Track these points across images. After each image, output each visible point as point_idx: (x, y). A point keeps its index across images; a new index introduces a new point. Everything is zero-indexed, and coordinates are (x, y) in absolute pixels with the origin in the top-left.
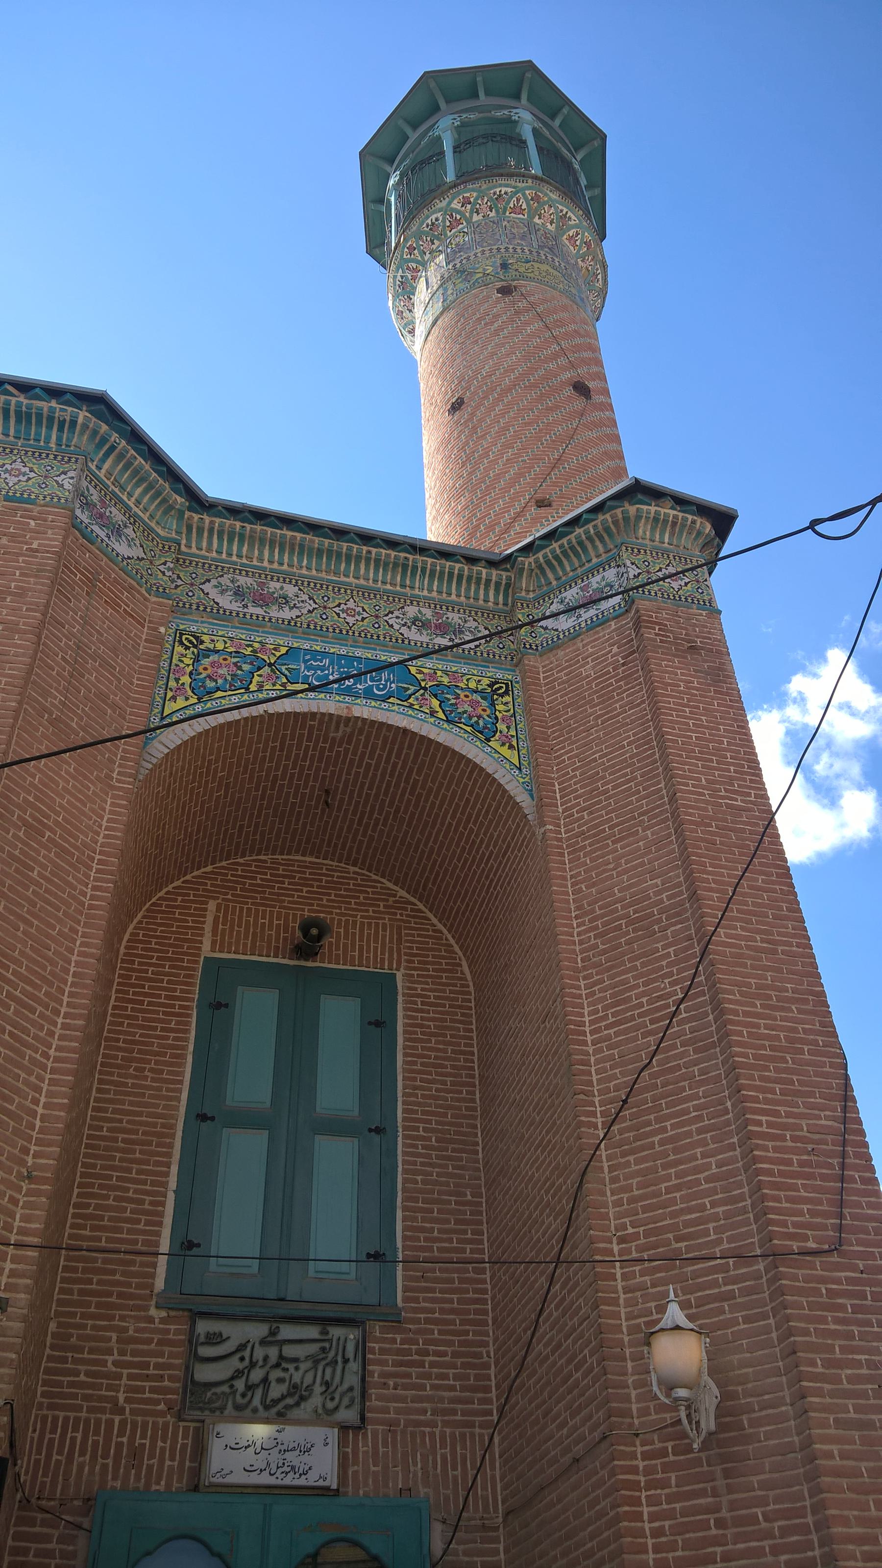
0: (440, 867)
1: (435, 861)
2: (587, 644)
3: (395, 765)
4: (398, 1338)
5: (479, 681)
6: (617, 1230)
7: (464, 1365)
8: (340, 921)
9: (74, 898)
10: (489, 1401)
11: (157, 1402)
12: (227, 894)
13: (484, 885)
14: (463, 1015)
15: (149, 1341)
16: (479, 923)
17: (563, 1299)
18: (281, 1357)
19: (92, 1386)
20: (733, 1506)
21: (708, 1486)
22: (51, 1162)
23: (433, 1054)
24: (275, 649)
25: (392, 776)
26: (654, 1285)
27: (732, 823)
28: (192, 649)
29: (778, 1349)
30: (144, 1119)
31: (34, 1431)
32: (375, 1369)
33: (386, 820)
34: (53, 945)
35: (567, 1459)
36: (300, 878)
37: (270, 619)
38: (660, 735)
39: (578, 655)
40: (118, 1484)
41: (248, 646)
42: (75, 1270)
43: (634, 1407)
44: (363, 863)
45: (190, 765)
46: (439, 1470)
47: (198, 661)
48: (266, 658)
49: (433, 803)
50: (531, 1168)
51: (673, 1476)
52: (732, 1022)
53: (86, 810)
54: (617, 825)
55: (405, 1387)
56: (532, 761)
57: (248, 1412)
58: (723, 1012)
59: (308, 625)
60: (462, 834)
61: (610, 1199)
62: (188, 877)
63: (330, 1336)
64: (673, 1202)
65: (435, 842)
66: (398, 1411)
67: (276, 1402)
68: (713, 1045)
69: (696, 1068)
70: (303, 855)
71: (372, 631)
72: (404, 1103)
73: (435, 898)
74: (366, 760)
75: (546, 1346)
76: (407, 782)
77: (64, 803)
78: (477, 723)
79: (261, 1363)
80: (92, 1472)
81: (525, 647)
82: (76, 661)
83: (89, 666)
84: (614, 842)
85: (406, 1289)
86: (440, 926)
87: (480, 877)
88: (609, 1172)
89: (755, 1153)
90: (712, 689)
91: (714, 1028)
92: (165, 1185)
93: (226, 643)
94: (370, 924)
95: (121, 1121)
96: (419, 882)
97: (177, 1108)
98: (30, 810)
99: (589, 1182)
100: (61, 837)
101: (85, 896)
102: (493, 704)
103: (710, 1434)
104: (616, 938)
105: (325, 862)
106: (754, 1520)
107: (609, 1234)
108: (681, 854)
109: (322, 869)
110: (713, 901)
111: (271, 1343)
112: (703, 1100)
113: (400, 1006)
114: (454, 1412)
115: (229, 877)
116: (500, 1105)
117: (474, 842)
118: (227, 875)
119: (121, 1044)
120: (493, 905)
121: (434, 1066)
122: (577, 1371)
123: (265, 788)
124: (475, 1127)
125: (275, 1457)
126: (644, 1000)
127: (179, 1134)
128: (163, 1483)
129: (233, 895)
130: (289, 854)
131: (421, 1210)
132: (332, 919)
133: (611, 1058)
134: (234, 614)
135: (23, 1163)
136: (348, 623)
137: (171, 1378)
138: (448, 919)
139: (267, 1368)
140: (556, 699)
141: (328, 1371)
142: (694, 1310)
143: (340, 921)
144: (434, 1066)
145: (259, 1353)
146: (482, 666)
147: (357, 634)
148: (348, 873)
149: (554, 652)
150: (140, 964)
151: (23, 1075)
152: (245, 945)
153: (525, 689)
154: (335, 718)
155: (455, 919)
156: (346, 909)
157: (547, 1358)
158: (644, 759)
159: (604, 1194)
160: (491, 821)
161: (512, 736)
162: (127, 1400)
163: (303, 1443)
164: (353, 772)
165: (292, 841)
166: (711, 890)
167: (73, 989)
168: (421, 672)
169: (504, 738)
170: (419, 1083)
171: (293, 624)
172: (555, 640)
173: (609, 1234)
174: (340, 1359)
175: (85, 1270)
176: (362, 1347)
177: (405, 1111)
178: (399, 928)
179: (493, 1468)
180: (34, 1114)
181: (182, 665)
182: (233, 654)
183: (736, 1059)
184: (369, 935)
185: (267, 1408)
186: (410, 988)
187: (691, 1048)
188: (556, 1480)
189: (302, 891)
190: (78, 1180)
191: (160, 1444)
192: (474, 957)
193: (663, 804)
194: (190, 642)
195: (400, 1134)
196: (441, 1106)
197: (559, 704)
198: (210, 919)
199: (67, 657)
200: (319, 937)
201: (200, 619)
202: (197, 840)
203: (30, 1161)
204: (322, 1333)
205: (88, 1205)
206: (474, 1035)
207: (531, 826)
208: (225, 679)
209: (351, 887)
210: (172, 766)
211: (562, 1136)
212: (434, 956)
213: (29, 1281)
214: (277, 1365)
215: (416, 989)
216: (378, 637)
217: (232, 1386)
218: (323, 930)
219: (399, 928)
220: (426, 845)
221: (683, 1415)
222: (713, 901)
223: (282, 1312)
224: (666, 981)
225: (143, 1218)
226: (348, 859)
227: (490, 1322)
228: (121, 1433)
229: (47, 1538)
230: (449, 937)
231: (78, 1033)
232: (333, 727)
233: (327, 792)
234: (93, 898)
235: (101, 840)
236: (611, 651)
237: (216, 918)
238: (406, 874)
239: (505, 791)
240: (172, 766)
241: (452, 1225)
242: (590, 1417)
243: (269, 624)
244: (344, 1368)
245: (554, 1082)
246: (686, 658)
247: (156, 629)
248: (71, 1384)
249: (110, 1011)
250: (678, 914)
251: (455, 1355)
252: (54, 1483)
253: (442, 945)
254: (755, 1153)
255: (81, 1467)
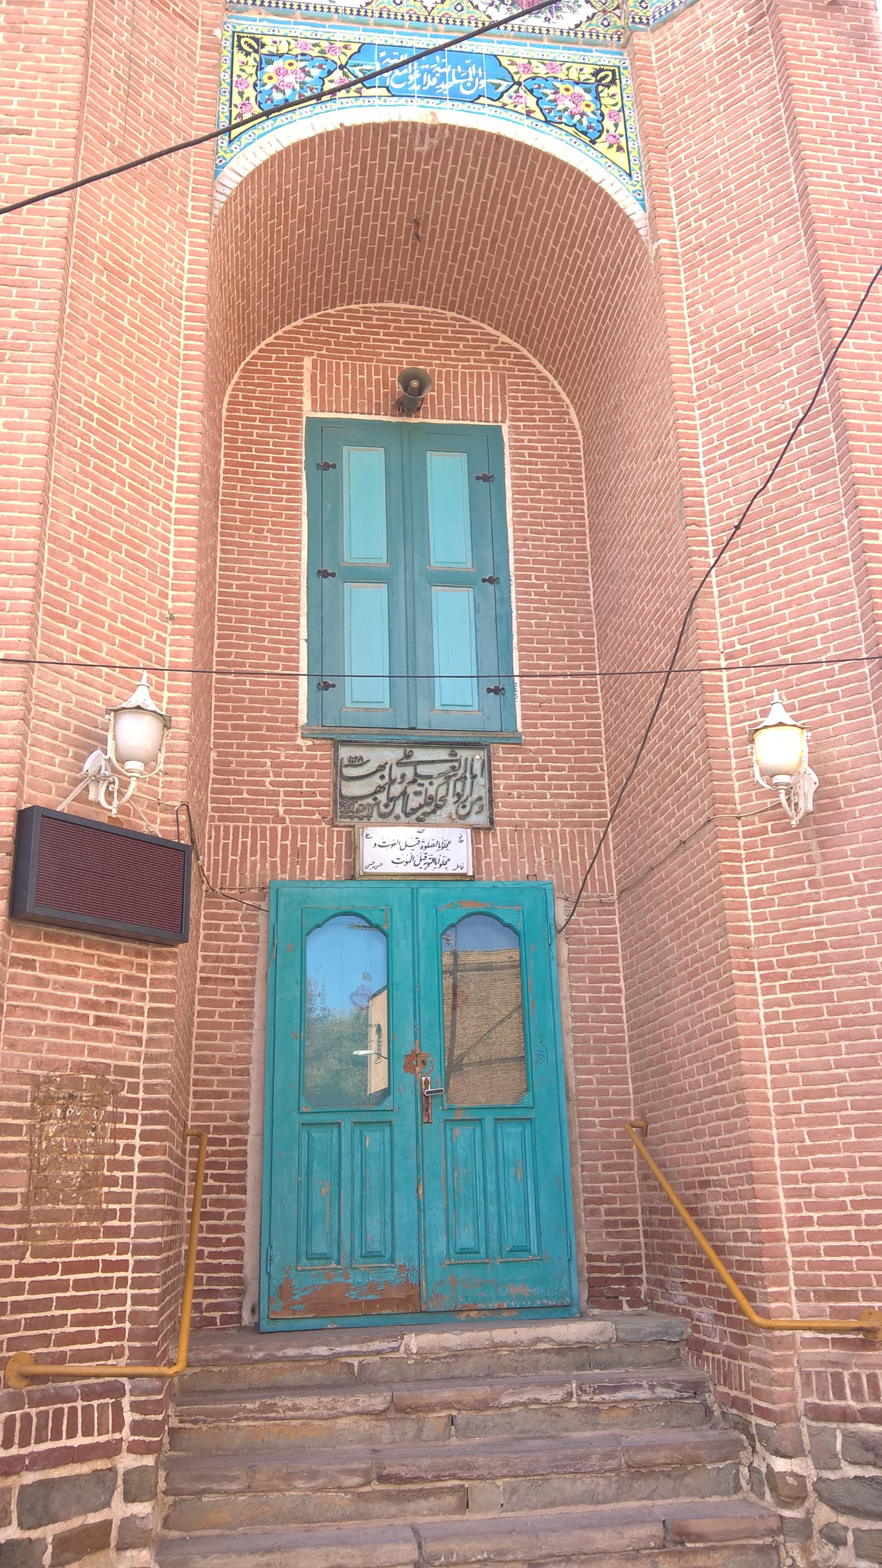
0: (544, 304)
1: (538, 297)
2: (707, 11)
3: (490, 181)
4: (520, 757)
5: (581, 70)
6: (725, 648)
7: (580, 778)
8: (440, 372)
9: (168, 348)
10: (604, 806)
11: (313, 813)
12: (321, 349)
13: (592, 318)
14: (571, 465)
15: (300, 765)
16: (587, 364)
17: (672, 712)
18: (416, 774)
19: (254, 802)
20: (826, 870)
21: (804, 855)
22: (189, 605)
23: (542, 506)
24: (346, 47)
25: (486, 197)
26: (758, 694)
27: (870, 218)
28: (253, 55)
29: (877, 740)
30: (269, 576)
31: (210, 838)
32: (501, 783)
33: (483, 252)
34: (156, 398)
35: (676, 842)
36: (395, 328)
37: (337, 9)
38: (792, 118)
39: (696, 26)
40: (287, 876)
41: (315, 45)
42: (226, 709)
43: (737, 796)
44: (461, 307)
45: (266, 197)
46: (560, 860)
47: (262, 69)
48: (336, 59)
49: (534, 227)
50: (641, 603)
51: (772, 849)
52: (855, 438)
53: (166, 251)
54: (740, 232)
55: (527, 796)
56: (643, 164)
57: (391, 819)
58: (846, 428)
59: (381, 14)
60: (567, 261)
61: (719, 620)
62: (280, 333)
63: (458, 758)
64: (782, 618)
65: (537, 275)
66: (522, 815)
67: (414, 810)
68: (833, 464)
69: (813, 489)
70: (397, 302)
71: (454, 14)
72: (515, 554)
73: (539, 342)
74: (457, 178)
75: (655, 754)
76: (503, 203)
77: (142, 243)
78: (580, 122)
79: (399, 780)
80: (263, 867)
81: (633, 22)
82: (130, 76)
83: (145, 82)
84: (736, 252)
85: (525, 717)
86: (546, 373)
87: (587, 311)
88: (720, 596)
89: (869, 565)
90: (855, 55)
91: (834, 446)
92: (297, 635)
93: (289, 44)
94: (471, 374)
95: (248, 579)
96: (521, 323)
97: (298, 566)
98: (108, 252)
99: (698, 607)
100: (145, 281)
101: (178, 345)
102: (598, 98)
103: (808, 814)
104: (736, 360)
105: (419, 308)
106: (846, 880)
107: (717, 652)
108: (811, 258)
109: (417, 316)
110: (843, 307)
111: (407, 764)
112: (818, 520)
113: (507, 460)
114: (572, 815)
115: (322, 330)
116: (610, 548)
117: (580, 269)
118: (318, 328)
119: (237, 507)
120: (602, 342)
121: (544, 517)
122: (683, 771)
123: (349, 221)
124: (587, 573)
125: (418, 852)
126: (762, 424)
127: (304, 590)
128: (324, 874)
129: (327, 350)
130: (381, 301)
131: (536, 650)
132: (433, 371)
133: (725, 487)
134: (295, 7)
135: (164, 606)
136: (426, 7)
137: (322, 794)
138: (553, 365)
139: (405, 784)
140: (671, 85)
141: (459, 785)
142: (797, 712)
143: (440, 372)
144: (544, 517)
145: (397, 772)
146: (585, 51)
147: (437, 21)
148: (446, 319)
149: (669, 25)
150: (244, 426)
151: (149, 526)
152: (346, 403)
153: (635, 76)
154: (419, 128)
155: (561, 363)
156: (446, 359)
157: (656, 764)
158: (772, 149)
159: (713, 616)
160: (599, 241)
161: (621, 136)
162: (286, 812)
163: (441, 841)
164: (443, 195)
165: (384, 285)
166: (841, 296)
167: (183, 442)
168: (513, 63)
169: (611, 138)
170: (529, 534)
171: (362, 13)
172: (670, 8)
173: (717, 652)
174: (468, 775)
175: (235, 709)
176: (488, 766)
177: (517, 561)
178: (503, 377)
179: (608, 858)
180: (166, 562)
181: (244, 75)
182: (299, 57)
183: (856, 475)
184: (471, 386)
185: (407, 815)
186: (516, 440)
187: (809, 469)
188: (665, 860)
189: (397, 342)
190: (216, 632)
191: (318, 845)
192: (582, 404)
193: (793, 201)
194: (250, 46)
195: (513, 583)
196: (552, 556)
197: (675, 91)
198: (307, 377)
199: (120, 72)
200: (420, 390)
201: (258, 17)
202: (284, 289)
203: (170, 604)
204: (451, 755)
205: (229, 655)
206: (584, 484)
207: (643, 243)
208: (294, 89)
209: (450, 334)
210: (247, 198)
211: (672, 568)
212: (540, 406)
213: (186, 707)
214: (414, 781)
215: (523, 441)
216: (462, 22)
217: (375, 799)
218: (424, 382)
219: (503, 377)
220: (527, 279)
221: (783, 798)
222: (843, 307)
223: (414, 739)
224: (787, 402)
225: (281, 663)
226: (444, 303)
227: (603, 742)
228: (284, 838)
229: (233, 917)
230: (556, 383)
231: (194, 486)
232: (417, 143)
233: (417, 222)
234: (187, 348)
235: (185, 284)
236: (735, 17)
237: (313, 376)
238: (508, 315)
239: (613, 203)
240: (247, 198)
241: (566, 662)
242: (697, 806)
243: (336, 16)
244: (472, 783)
245: (666, 517)
246: (825, 17)
247: (210, 33)
248: (236, 801)
249: (222, 475)
250: (804, 328)
251: (571, 769)
252: (233, 877)
253: (549, 393)
254: (869, 565)
255: (254, 864)
